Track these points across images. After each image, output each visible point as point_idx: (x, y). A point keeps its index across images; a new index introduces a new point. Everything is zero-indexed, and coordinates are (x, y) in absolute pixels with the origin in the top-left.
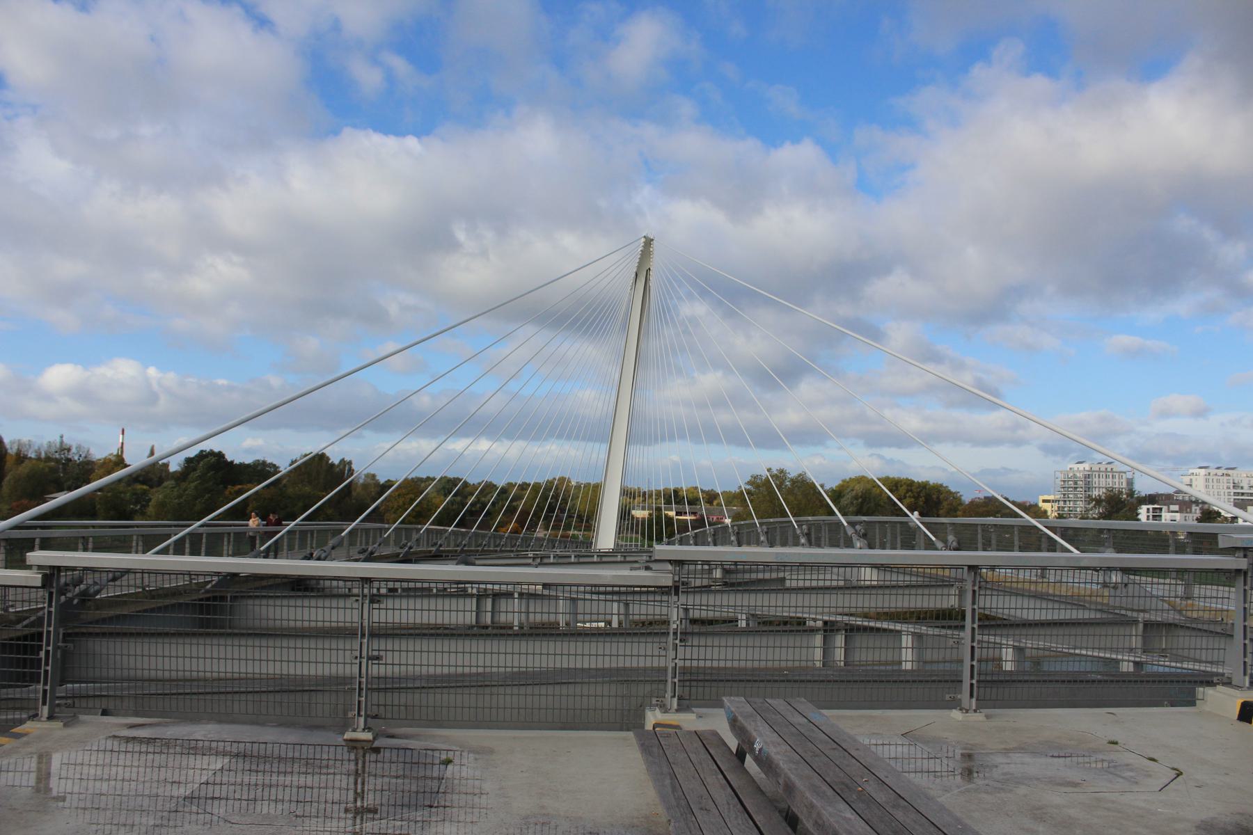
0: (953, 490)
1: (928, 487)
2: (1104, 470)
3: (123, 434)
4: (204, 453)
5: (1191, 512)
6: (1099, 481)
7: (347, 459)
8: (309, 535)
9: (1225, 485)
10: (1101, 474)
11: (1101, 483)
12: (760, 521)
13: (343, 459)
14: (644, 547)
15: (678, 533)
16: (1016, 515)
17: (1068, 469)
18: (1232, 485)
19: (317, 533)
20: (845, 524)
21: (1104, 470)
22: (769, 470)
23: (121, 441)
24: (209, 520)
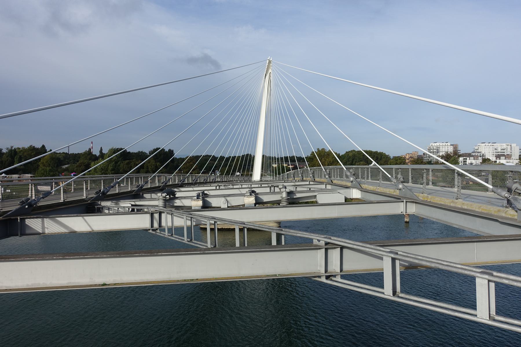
0: (387, 154)
1: (377, 153)
2: (444, 145)
3: (92, 143)
4: (119, 149)
5: (478, 160)
6: (442, 149)
7: (172, 149)
8: (140, 179)
9: (492, 149)
10: (443, 146)
11: (443, 150)
12: (310, 168)
13: (2, 149)
14: (142, 194)
15: (282, 173)
17: (431, 145)
18: (494, 149)
19: (143, 178)
21: (444, 145)
23: (92, 146)
24: (81, 176)
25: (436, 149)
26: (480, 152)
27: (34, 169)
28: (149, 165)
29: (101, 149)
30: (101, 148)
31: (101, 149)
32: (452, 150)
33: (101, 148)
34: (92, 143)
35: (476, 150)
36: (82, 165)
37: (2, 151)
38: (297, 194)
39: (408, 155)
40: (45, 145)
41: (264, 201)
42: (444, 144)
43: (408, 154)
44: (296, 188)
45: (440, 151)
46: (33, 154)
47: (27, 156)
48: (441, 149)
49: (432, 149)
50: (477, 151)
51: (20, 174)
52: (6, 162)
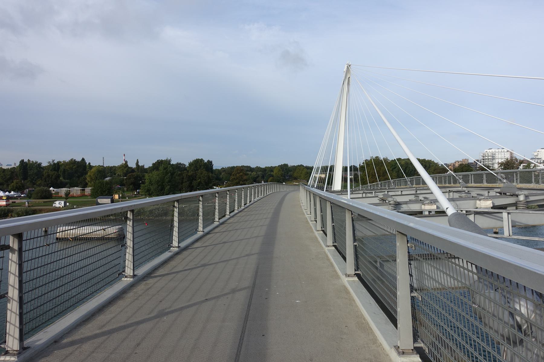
3: (125, 156)
7: (210, 160)
8: (515, 175)
10: (499, 153)
13: (42, 163)
16: (486, 170)
17: (485, 152)
20: (455, 176)
22: (53, 161)
23: (124, 158)
25: (491, 156)
26: (540, 159)
27: (81, 182)
28: (201, 176)
29: (138, 162)
30: (138, 160)
31: (138, 162)
32: (509, 156)
33: (138, 160)
34: (125, 156)
35: (536, 157)
36: (132, 178)
37: (42, 165)
38: (530, 197)
39: (457, 162)
40: (84, 158)
41: (495, 205)
42: (500, 150)
43: (458, 161)
44: (489, 192)
45: (496, 158)
46: (74, 167)
47: (69, 170)
48: (496, 155)
49: (487, 155)
50: (537, 157)
51: (69, 188)
52: (52, 175)
